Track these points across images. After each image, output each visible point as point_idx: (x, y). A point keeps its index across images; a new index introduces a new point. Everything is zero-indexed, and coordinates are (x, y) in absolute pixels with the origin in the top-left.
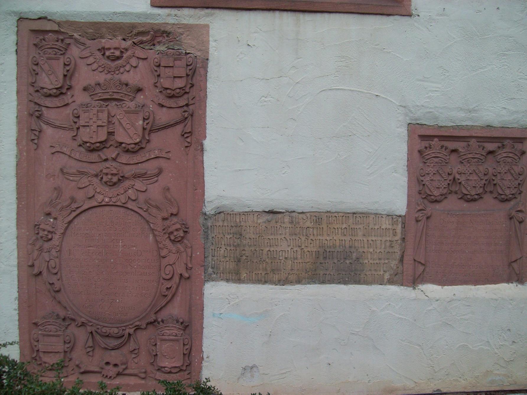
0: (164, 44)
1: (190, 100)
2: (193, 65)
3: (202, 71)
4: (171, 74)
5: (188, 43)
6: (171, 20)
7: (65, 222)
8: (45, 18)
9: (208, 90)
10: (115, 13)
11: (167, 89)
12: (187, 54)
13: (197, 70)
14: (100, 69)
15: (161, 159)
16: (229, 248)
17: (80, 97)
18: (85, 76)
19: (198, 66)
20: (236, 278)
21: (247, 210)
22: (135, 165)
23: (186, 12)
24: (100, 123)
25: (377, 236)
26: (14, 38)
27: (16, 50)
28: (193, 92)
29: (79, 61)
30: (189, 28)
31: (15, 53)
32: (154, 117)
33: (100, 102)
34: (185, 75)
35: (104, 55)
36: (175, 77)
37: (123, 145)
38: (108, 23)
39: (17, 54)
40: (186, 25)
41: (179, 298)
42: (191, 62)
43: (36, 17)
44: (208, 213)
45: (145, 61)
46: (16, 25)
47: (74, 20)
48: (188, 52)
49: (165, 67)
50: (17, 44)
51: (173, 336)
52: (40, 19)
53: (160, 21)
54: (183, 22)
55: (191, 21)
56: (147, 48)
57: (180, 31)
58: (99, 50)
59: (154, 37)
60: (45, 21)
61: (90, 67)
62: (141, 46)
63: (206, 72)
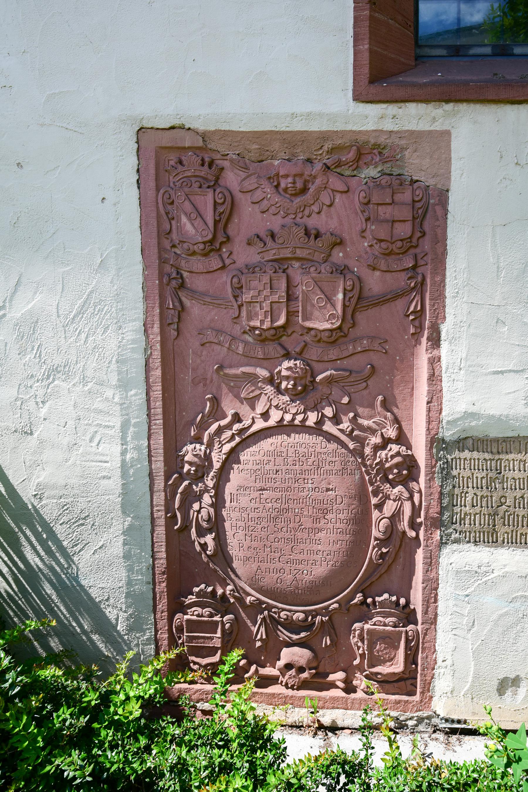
0: (375, 167)
1: (419, 258)
2: (424, 200)
3: (439, 210)
4: (388, 216)
5: (417, 166)
6: (388, 126)
7: (223, 452)
8: (182, 127)
9: (448, 242)
10: (293, 116)
11: (381, 241)
12: (413, 182)
13: (430, 207)
14: (273, 210)
15: (371, 353)
16: (479, 494)
17: (243, 254)
18: (250, 219)
19: (432, 201)
20: (490, 538)
21: (510, 434)
22: (331, 363)
23: (412, 108)
24: (275, 298)
25: (153, 324)
26: (133, 161)
27: (138, 181)
28: (426, 244)
29: (239, 196)
30: (416, 136)
31: (136, 185)
32: (361, 288)
33: (273, 263)
34: (411, 218)
35: (277, 187)
36: (394, 221)
37: (313, 333)
38: (284, 132)
39: (139, 188)
40: (412, 133)
41: (399, 567)
42: (421, 196)
43: (168, 126)
44: (447, 439)
45: (344, 195)
46: (135, 139)
47: (227, 128)
48: (415, 178)
49: (378, 204)
50: (138, 171)
51: (390, 626)
52: (172, 128)
53: (370, 126)
54: (407, 128)
55: (424, 126)
56: (348, 173)
57: (403, 142)
58: (269, 178)
59: (360, 155)
60: (182, 132)
61: (257, 206)
62: (338, 170)
63: (446, 212)
